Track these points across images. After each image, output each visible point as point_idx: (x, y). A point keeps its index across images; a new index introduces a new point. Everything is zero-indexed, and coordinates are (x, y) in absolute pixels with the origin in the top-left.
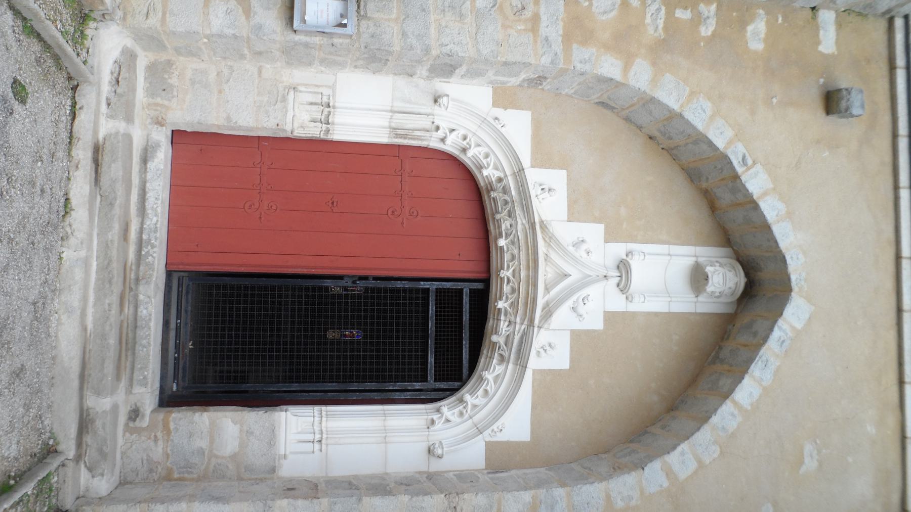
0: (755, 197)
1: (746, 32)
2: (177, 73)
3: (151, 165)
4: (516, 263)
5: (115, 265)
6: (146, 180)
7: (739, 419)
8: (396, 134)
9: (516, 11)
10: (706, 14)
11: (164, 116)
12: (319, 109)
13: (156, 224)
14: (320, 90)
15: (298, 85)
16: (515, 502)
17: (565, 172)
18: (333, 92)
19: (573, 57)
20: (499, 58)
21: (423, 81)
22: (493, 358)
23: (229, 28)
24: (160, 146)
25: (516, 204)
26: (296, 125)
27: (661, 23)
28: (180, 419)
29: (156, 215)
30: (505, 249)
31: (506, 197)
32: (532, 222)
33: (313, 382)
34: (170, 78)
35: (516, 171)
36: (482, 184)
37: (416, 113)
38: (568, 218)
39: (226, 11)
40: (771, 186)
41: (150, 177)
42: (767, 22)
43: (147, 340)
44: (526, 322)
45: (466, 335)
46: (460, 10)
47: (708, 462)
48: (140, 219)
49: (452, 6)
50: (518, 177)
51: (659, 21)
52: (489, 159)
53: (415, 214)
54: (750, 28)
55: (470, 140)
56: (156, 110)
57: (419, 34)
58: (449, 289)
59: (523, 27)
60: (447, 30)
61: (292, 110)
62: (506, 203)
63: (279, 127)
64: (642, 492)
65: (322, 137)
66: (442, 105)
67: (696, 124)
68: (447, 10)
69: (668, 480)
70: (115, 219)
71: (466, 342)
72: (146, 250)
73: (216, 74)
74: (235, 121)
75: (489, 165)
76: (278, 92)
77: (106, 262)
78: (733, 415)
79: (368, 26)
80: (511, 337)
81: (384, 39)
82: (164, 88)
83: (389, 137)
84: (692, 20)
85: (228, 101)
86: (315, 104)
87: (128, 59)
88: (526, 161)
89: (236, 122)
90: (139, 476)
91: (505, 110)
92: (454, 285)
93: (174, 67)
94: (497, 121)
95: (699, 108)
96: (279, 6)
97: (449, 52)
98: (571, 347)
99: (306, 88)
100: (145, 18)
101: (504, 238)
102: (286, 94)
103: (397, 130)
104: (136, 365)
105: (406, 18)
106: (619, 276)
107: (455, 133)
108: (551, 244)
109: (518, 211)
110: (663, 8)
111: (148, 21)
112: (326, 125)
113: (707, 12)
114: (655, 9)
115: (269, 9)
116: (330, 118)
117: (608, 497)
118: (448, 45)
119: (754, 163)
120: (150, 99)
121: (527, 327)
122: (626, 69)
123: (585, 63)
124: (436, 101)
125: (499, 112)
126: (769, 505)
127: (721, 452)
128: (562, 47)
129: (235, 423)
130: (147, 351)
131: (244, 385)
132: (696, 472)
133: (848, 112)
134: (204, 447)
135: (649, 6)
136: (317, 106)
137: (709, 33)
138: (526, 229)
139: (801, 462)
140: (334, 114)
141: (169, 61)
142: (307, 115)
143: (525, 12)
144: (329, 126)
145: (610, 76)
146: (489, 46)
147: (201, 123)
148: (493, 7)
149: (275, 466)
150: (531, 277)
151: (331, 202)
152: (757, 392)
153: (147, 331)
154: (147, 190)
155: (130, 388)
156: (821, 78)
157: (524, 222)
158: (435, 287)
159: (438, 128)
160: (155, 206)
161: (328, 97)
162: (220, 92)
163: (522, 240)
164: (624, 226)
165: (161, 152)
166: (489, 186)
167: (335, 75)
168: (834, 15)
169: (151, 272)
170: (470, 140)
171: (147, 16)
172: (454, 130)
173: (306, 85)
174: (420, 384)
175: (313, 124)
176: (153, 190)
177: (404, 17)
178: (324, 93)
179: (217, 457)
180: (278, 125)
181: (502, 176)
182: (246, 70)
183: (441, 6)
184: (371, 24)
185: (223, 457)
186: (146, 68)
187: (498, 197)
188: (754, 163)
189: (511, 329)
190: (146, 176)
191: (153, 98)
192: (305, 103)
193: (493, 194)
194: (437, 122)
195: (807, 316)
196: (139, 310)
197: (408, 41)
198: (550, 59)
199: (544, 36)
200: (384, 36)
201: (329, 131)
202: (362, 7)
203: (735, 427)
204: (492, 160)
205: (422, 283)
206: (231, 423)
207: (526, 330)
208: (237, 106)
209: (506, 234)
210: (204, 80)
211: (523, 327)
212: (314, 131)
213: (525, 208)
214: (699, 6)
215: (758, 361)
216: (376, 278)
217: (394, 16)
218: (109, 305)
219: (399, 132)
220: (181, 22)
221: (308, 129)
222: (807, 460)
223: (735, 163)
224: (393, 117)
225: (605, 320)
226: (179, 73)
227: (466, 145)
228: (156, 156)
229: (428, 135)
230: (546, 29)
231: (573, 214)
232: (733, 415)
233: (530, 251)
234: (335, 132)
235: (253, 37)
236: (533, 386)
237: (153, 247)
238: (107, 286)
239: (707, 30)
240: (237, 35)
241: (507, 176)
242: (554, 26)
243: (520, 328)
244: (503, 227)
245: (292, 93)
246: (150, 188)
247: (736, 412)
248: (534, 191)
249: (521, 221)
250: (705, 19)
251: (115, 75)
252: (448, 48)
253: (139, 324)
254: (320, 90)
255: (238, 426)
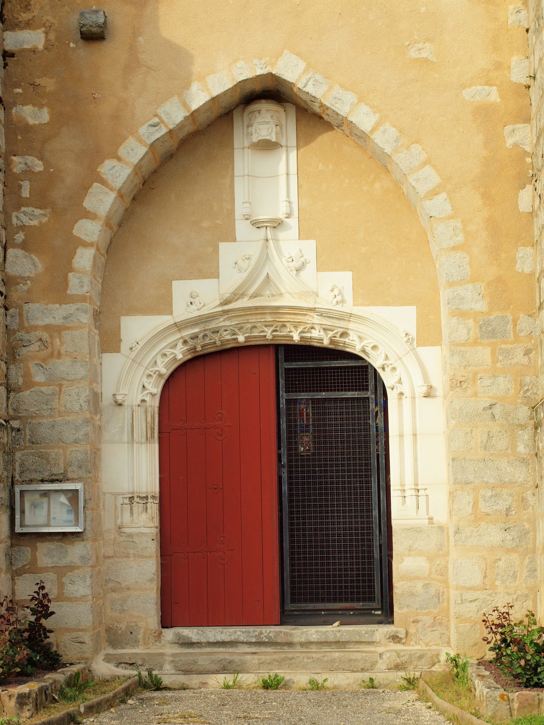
0: (188, 114)
1: (35, 125)
2: (116, 623)
3: (195, 639)
4: (259, 325)
5: (275, 657)
6: (207, 642)
7: (387, 126)
8: (151, 437)
9: (44, 347)
10: (23, 166)
11: (154, 631)
12: (136, 506)
13: (243, 632)
14: (119, 506)
15: (116, 525)
16: (457, 331)
17: (175, 283)
18: (120, 495)
19: (78, 294)
20: (87, 360)
21: (103, 417)
22: (345, 342)
23: (85, 581)
24: (178, 633)
25: (207, 328)
26: (152, 525)
27: (38, 212)
28: (400, 603)
29: (236, 632)
30: (247, 335)
31: (201, 336)
32: (222, 312)
33: (372, 497)
34: (121, 629)
35: (177, 329)
36: (189, 357)
37: (131, 421)
38: (216, 278)
39: (72, 584)
40: (175, 99)
41: (204, 640)
42: (23, 105)
43: (337, 633)
44: (312, 314)
45: (326, 364)
46: (49, 395)
47: (426, 155)
48: (240, 644)
49: (47, 402)
50: (182, 327)
51: (35, 213)
52: (168, 354)
53: (220, 415)
54: (31, 121)
55: (152, 371)
56: (149, 638)
57: (74, 429)
58: (285, 382)
59: (58, 340)
60: (68, 406)
61: (140, 529)
62: (205, 336)
63: (155, 538)
64: (450, 218)
65: (158, 501)
66: (124, 399)
67: (127, 175)
68: (50, 407)
69: (440, 193)
70: (242, 658)
71: (333, 363)
72: (264, 638)
73: (113, 593)
74: (153, 575)
75: (173, 353)
76: (124, 541)
77: (276, 663)
78: (384, 132)
79: (72, 471)
80: (325, 327)
81: (81, 458)
82: (129, 633)
83: (154, 444)
84: (30, 180)
85: (136, 582)
86: (131, 509)
87: (108, 659)
88: (165, 320)
89: (154, 574)
90: (445, 632)
91: (122, 341)
92: (282, 377)
93: (111, 626)
94: (133, 349)
95: (111, 172)
96: (63, 544)
97: (87, 403)
98: (332, 271)
99: (118, 518)
100: (84, 644)
101: (238, 337)
102: (126, 534)
103: (148, 437)
104: (357, 640)
105: (62, 441)
106: (266, 228)
107: (146, 385)
108: (240, 293)
109: (213, 325)
110: (23, 209)
111: (87, 642)
112: (149, 499)
113: (21, 165)
114: (25, 217)
115: (66, 551)
116: (142, 496)
117: (455, 248)
118: (80, 404)
119: (156, 115)
120: (140, 643)
121: (316, 313)
122: (86, 245)
123: (82, 282)
124: (120, 405)
125: (124, 347)
126: (464, 92)
127: (417, 142)
128: (71, 305)
129: (403, 560)
130: (345, 632)
131: (375, 556)
132: (434, 167)
133: (103, 26)
134: (422, 584)
135: (22, 222)
136: (134, 508)
137: (41, 163)
138: (229, 317)
139: (426, 61)
140: (139, 493)
141: (106, 630)
142: (141, 516)
143: (44, 338)
144: (149, 497)
145: (91, 259)
146: (78, 369)
147: (157, 602)
148: (43, 367)
149: (438, 526)
150: (272, 311)
151: (215, 491)
152: (364, 108)
153: (330, 633)
154: (215, 641)
155: (375, 644)
156: (69, 46)
157: (222, 319)
158: (285, 394)
159: (143, 401)
160: (228, 633)
161: (125, 499)
162: (128, 589)
163: (238, 321)
164: (219, 222)
165: (183, 632)
166: (191, 351)
167: (104, 494)
168: (7, 32)
169: (282, 633)
170: (152, 371)
171: (83, 643)
172: (144, 386)
173: (116, 518)
174: (370, 404)
175: (149, 510)
176: (215, 636)
177: (61, 443)
178: (121, 502)
179: (430, 574)
180: (153, 540)
181: (182, 341)
182: (108, 569)
183: (48, 411)
184: (70, 469)
185: (431, 569)
186: (115, 649)
187: (201, 344)
188: (156, 115)
189: (317, 327)
190: (204, 643)
191: (139, 641)
192: (131, 518)
193: (199, 348)
194: (139, 402)
195: (294, 56)
196: (313, 640)
197: (81, 438)
198: (82, 314)
199: (63, 321)
200: (79, 458)
201: (153, 496)
202: (57, 478)
203: (394, 129)
204: (168, 351)
205: (281, 406)
206: (403, 563)
207: (319, 314)
208: (139, 574)
209: (234, 334)
210: (120, 602)
211: (316, 316)
212: (154, 508)
213: (208, 319)
214: (16, 173)
215: (336, 107)
216: (279, 448)
217: (61, 451)
218: (308, 659)
219: (149, 435)
220: (84, 618)
221: (153, 514)
222: (424, 55)
223: (158, 135)
224: (137, 441)
225: (307, 238)
226: (116, 622)
227: (156, 375)
228: (186, 636)
229: (150, 409)
230: (57, 319)
231: (212, 273)
232: (384, 132)
233: (248, 313)
234: (153, 491)
235: (91, 563)
236: (368, 305)
237: (261, 633)
238: (294, 661)
239: (38, 166)
240: (90, 575)
241: (182, 337)
242: (53, 311)
243: (316, 319)
244: (228, 337)
245: (124, 530)
246: (213, 638)
247: (382, 128)
248: (194, 313)
249: (221, 323)
250: (28, 167)
251: (127, 666)
252: (83, 404)
253: (323, 640)
254: (119, 506)
255: (404, 558)
